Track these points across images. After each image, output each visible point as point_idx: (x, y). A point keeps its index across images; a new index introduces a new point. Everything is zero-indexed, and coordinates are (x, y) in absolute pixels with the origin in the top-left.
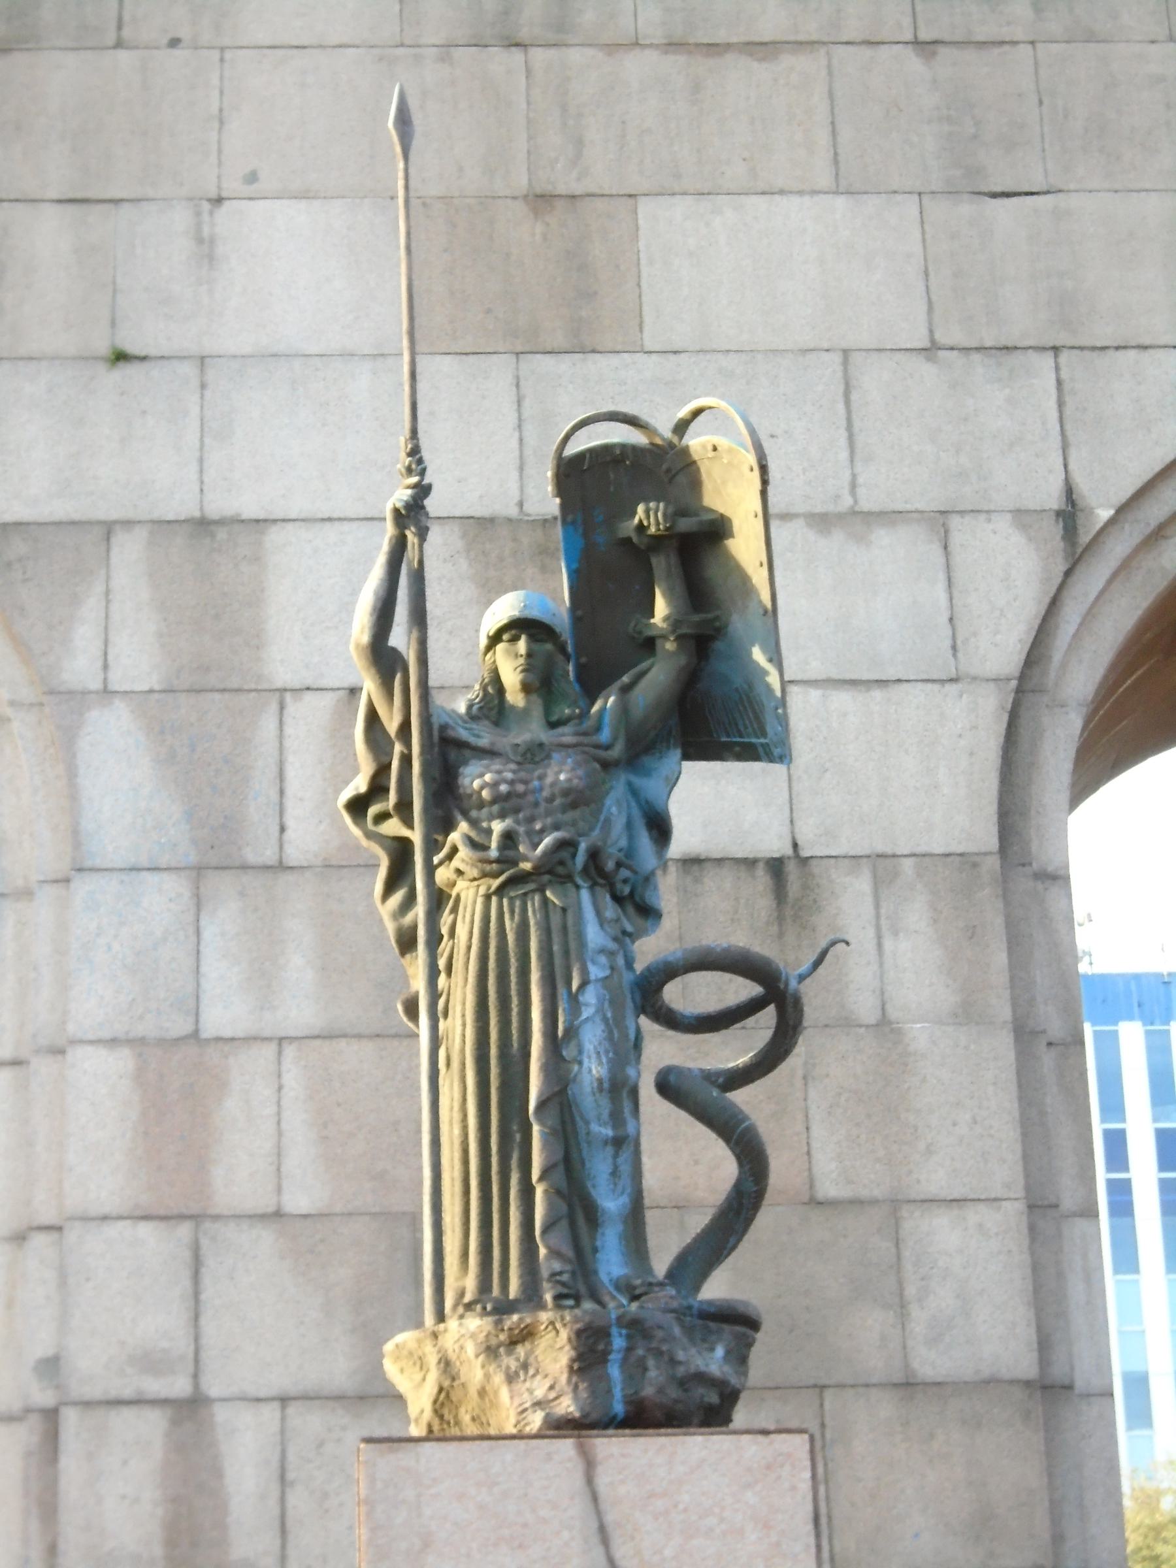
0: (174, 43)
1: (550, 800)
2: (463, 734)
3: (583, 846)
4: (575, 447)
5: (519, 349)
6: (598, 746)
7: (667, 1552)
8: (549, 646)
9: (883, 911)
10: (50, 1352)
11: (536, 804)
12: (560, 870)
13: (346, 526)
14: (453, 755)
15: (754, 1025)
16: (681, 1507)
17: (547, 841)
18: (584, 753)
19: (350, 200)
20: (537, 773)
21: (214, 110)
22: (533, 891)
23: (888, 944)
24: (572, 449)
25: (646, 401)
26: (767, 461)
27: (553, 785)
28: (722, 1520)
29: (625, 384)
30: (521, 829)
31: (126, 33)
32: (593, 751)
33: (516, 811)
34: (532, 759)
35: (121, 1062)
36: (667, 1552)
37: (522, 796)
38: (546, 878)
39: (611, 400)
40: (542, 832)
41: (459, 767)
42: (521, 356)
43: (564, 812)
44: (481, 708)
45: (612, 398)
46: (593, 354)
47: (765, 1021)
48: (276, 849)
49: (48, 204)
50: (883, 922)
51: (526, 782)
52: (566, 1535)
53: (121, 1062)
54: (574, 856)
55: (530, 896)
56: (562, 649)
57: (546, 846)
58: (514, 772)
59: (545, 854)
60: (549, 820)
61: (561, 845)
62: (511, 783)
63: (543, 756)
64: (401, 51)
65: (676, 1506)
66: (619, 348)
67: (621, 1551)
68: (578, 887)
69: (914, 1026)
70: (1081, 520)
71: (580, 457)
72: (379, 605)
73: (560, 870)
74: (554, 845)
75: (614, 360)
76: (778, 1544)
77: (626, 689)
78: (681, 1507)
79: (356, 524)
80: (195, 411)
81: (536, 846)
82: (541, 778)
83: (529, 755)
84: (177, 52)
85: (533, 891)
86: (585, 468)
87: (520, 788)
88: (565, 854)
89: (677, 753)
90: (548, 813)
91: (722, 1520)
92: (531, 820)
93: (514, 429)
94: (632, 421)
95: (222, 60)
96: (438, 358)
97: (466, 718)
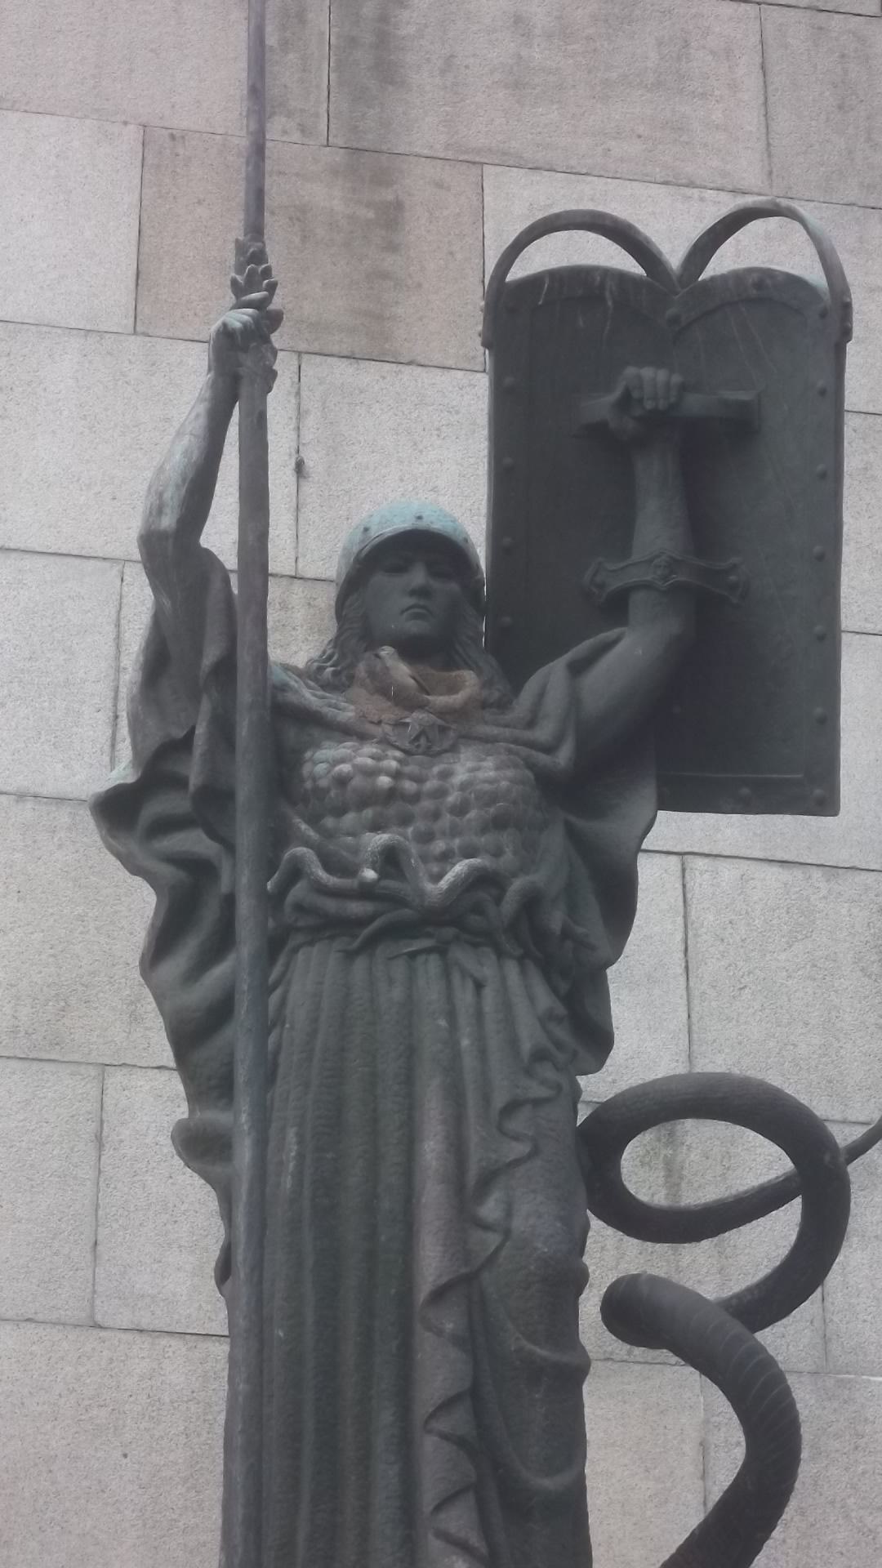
1: (460, 810)
2: (309, 696)
3: (517, 885)
5: (302, 346)
6: (532, 745)
8: (454, 587)
11: (436, 815)
12: (474, 920)
13: (28, 562)
14: (291, 734)
15: (626, 1357)
17: (460, 868)
19: (63, 119)
20: (436, 770)
24: (518, 271)
26: (851, 299)
27: (463, 787)
30: (414, 849)
32: (524, 751)
33: (405, 820)
34: (429, 748)
38: (449, 932)
39: (436, 432)
40: (446, 858)
42: (305, 357)
43: (484, 830)
45: (438, 429)
51: (420, 780)
54: (498, 901)
55: (421, 959)
57: (457, 876)
58: (399, 761)
59: (453, 887)
60: (457, 842)
61: (480, 880)
62: (397, 775)
63: (446, 744)
68: (500, 954)
69: (872, 1379)
71: (533, 283)
72: (190, 475)
73: (474, 920)
74: (468, 875)
75: (439, 377)
77: (578, 669)
79: (41, 561)
81: (437, 878)
82: (446, 775)
83: (423, 741)
85: (428, 951)
86: (540, 303)
87: (409, 786)
88: (483, 895)
89: (648, 792)
90: (454, 832)
92: (426, 838)
96: (182, 345)
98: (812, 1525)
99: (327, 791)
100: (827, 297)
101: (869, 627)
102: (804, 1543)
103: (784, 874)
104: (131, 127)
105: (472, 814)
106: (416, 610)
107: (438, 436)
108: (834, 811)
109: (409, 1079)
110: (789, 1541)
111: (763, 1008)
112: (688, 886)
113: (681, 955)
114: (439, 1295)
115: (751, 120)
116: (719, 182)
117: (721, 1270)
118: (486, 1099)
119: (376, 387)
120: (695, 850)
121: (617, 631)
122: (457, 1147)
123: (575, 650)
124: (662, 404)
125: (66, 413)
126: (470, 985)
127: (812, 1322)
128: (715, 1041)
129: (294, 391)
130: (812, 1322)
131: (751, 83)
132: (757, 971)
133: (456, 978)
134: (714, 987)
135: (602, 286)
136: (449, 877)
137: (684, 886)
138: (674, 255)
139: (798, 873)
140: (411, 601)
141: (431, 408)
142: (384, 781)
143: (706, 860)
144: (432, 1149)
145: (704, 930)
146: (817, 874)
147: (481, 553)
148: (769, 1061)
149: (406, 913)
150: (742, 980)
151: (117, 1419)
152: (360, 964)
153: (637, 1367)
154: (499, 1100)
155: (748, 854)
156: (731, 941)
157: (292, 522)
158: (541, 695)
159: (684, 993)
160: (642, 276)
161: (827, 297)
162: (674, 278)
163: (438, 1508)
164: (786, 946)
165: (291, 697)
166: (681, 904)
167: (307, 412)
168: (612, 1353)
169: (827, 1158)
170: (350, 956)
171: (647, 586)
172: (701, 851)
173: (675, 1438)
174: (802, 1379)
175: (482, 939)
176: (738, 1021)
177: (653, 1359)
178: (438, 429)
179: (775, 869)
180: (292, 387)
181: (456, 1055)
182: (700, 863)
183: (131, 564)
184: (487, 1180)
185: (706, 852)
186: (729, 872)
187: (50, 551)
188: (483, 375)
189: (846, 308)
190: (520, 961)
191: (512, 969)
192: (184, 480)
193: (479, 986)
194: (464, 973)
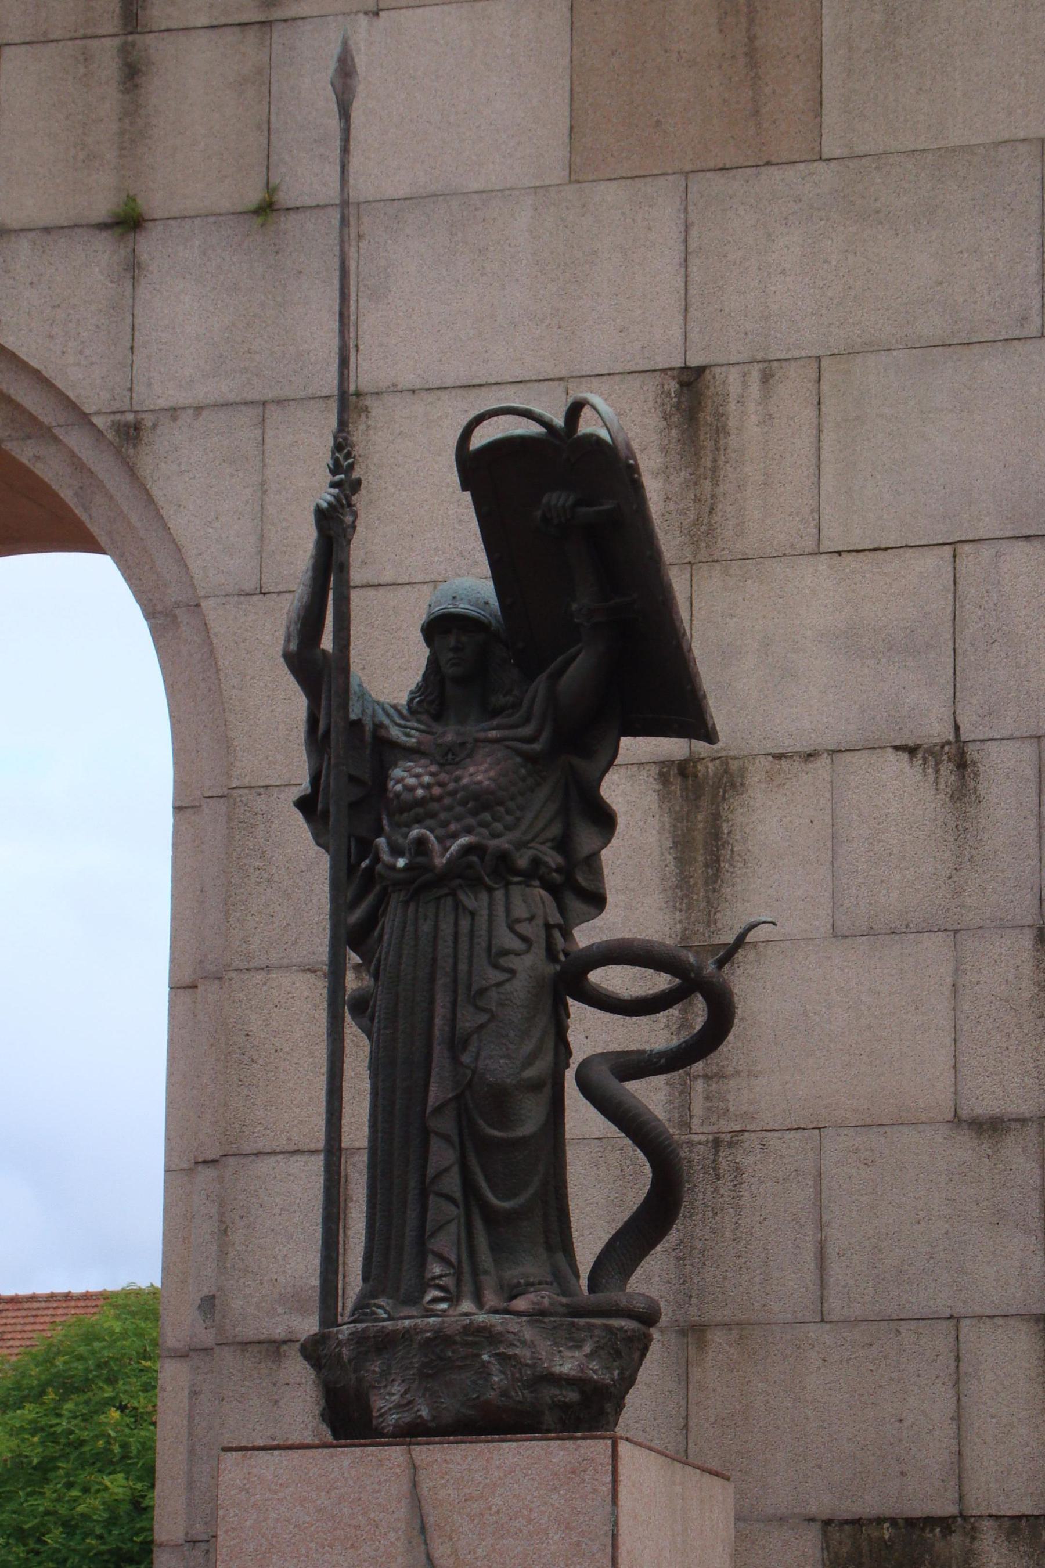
2: (395, 733)
4: (480, 439)
5: (688, 167)
7: (480, 1552)
15: (904, 930)
16: (494, 1509)
17: (464, 840)
18: (508, 747)
22: (446, 895)
25: (821, 220)
29: (800, 201)
35: (1028, 750)
36: (480, 1552)
37: (439, 799)
38: (458, 881)
39: (785, 222)
40: (455, 836)
41: (388, 770)
42: (691, 175)
44: (419, 703)
45: (786, 219)
46: (769, 168)
47: (698, 1012)
49: (201, 32)
52: (392, 1536)
53: (1028, 750)
65: (490, 1508)
66: (795, 158)
67: (440, 1550)
68: (490, 890)
72: (302, 614)
75: (790, 172)
78: (494, 1509)
83: (450, 756)
85: (446, 895)
91: (530, 1521)
93: (680, 264)
94: (527, 414)
97: (405, 712)
98: (1027, 1035)
102: (1020, 1048)
106: (454, 661)
107: (786, 224)
109: (432, 980)
110: (1010, 1047)
111: (1007, 656)
112: (957, 568)
113: (951, 624)
118: (469, 988)
119: (742, 191)
120: (963, 538)
123: (552, 666)
125: (524, 262)
127: (1032, 889)
128: (972, 687)
129: (682, 207)
130: (1032, 889)
132: (1004, 627)
134: (973, 645)
136: (454, 848)
137: (955, 568)
138: (559, 421)
140: (451, 655)
141: (780, 201)
142: (420, 792)
143: (971, 545)
145: (967, 601)
148: (1010, 696)
149: (428, 876)
150: (994, 636)
151: (581, 1013)
153: (912, 936)
155: (1000, 534)
156: (986, 606)
157: (682, 322)
158: (536, 691)
159: (952, 653)
160: (540, 434)
162: (563, 434)
164: (1026, 604)
165: (383, 732)
166: (952, 583)
167: (692, 224)
168: (895, 928)
169: (693, 975)
172: (967, 538)
173: (936, 984)
174: (1024, 931)
176: (988, 669)
177: (923, 928)
178: (786, 219)
180: (681, 204)
182: (967, 548)
183: (572, 379)
185: (971, 539)
186: (986, 552)
187: (518, 380)
192: (299, 619)
194: (465, 908)
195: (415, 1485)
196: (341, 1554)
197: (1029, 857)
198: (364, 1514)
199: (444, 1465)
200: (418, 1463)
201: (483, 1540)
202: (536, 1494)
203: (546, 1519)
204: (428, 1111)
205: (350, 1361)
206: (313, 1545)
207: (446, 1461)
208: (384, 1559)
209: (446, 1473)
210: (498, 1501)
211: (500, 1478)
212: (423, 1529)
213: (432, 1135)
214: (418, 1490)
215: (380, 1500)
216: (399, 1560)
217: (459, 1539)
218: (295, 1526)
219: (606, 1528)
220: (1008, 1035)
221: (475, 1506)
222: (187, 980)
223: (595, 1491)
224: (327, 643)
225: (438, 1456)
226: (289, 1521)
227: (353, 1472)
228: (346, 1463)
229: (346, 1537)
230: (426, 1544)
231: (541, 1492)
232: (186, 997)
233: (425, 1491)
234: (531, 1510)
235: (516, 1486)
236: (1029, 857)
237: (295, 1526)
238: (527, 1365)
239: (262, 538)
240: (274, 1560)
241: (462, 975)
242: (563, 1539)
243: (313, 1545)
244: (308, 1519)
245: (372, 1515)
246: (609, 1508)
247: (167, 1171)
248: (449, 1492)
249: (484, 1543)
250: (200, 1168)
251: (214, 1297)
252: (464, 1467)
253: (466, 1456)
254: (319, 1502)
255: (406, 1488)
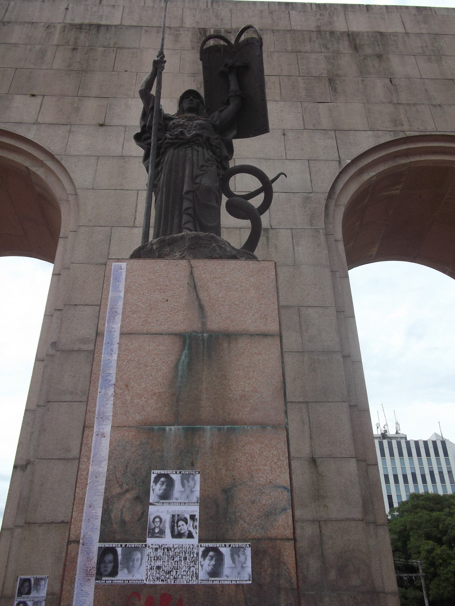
0: (126, 71)
8: (198, 100)
9: (294, 240)
10: (56, 341)
16: (226, 282)
21: (134, 83)
23: (296, 248)
28: (241, 286)
31: (115, 69)
38: (193, 143)
48: (133, 223)
50: (294, 243)
55: (188, 148)
56: (202, 102)
61: (197, 135)
64: (179, 74)
65: (224, 281)
68: (203, 148)
70: (342, 162)
72: (147, 81)
73: (197, 142)
76: (263, 294)
77: (221, 111)
78: (226, 282)
80: (123, 136)
83: (190, 119)
84: (127, 73)
85: (189, 147)
95: (137, 74)
99: (171, 126)
100: (258, 39)
101: (299, 159)
103: (286, 194)
104: (176, 100)
105: (198, 127)
108: (268, 132)
109: (184, 164)
114: (187, 192)
115: (278, 91)
116: (273, 100)
117: (276, 251)
121: (227, 106)
122: (192, 172)
124: (232, 64)
126: (196, 151)
131: (278, 86)
133: (194, 150)
135: (220, 48)
139: (288, 194)
144: (187, 172)
146: (291, 194)
147: (202, 93)
152: (176, 151)
154: (200, 165)
161: (258, 39)
163: (184, 224)
169: (266, 179)
170: (175, 149)
171: (232, 96)
175: (199, 145)
179: (284, 193)
181: (193, 159)
184: (197, 177)
188: (395, 433)
189: (261, 39)
190: (207, 149)
191: (205, 150)
193: (198, 151)
194: (195, 149)
195: (192, 273)
196: (158, 294)
197: (291, 252)
198: (169, 281)
199: (204, 267)
200: (193, 266)
201: (221, 291)
202: (243, 277)
203: (249, 286)
204: (184, 192)
205: (156, 249)
206: (146, 291)
207: (205, 266)
208: (178, 296)
209: (205, 269)
210: (228, 279)
211: (228, 272)
212: (195, 287)
213: (184, 200)
214: (193, 274)
215: (176, 277)
216: (184, 297)
217: (211, 291)
218: (138, 284)
219: (274, 289)
220: (288, 288)
221: (218, 280)
222: (57, 273)
223: (269, 277)
224: (153, 92)
225: (202, 264)
226: (136, 282)
227: (165, 267)
228: (162, 265)
229: (161, 289)
230: (196, 292)
231: (246, 277)
232: (56, 277)
233: (196, 275)
234: (242, 282)
235: (235, 275)
236: (291, 252)
237: (138, 284)
238: (228, 252)
239: (94, 179)
240: (128, 295)
241: (195, 161)
242: (256, 292)
243: (146, 291)
244: (144, 282)
245: (173, 282)
246: (275, 283)
247: (45, 315)
248: (206, 275)
249: (222, 293)
250: (56, 311)
251: (55, 342)
252: (213, 268)
253: (214, 264)
254: (149, 277)
255: (188, 273)
